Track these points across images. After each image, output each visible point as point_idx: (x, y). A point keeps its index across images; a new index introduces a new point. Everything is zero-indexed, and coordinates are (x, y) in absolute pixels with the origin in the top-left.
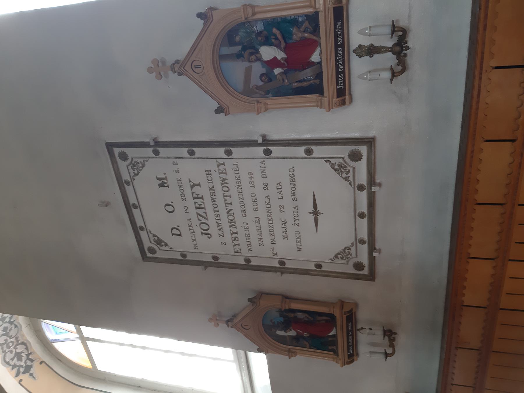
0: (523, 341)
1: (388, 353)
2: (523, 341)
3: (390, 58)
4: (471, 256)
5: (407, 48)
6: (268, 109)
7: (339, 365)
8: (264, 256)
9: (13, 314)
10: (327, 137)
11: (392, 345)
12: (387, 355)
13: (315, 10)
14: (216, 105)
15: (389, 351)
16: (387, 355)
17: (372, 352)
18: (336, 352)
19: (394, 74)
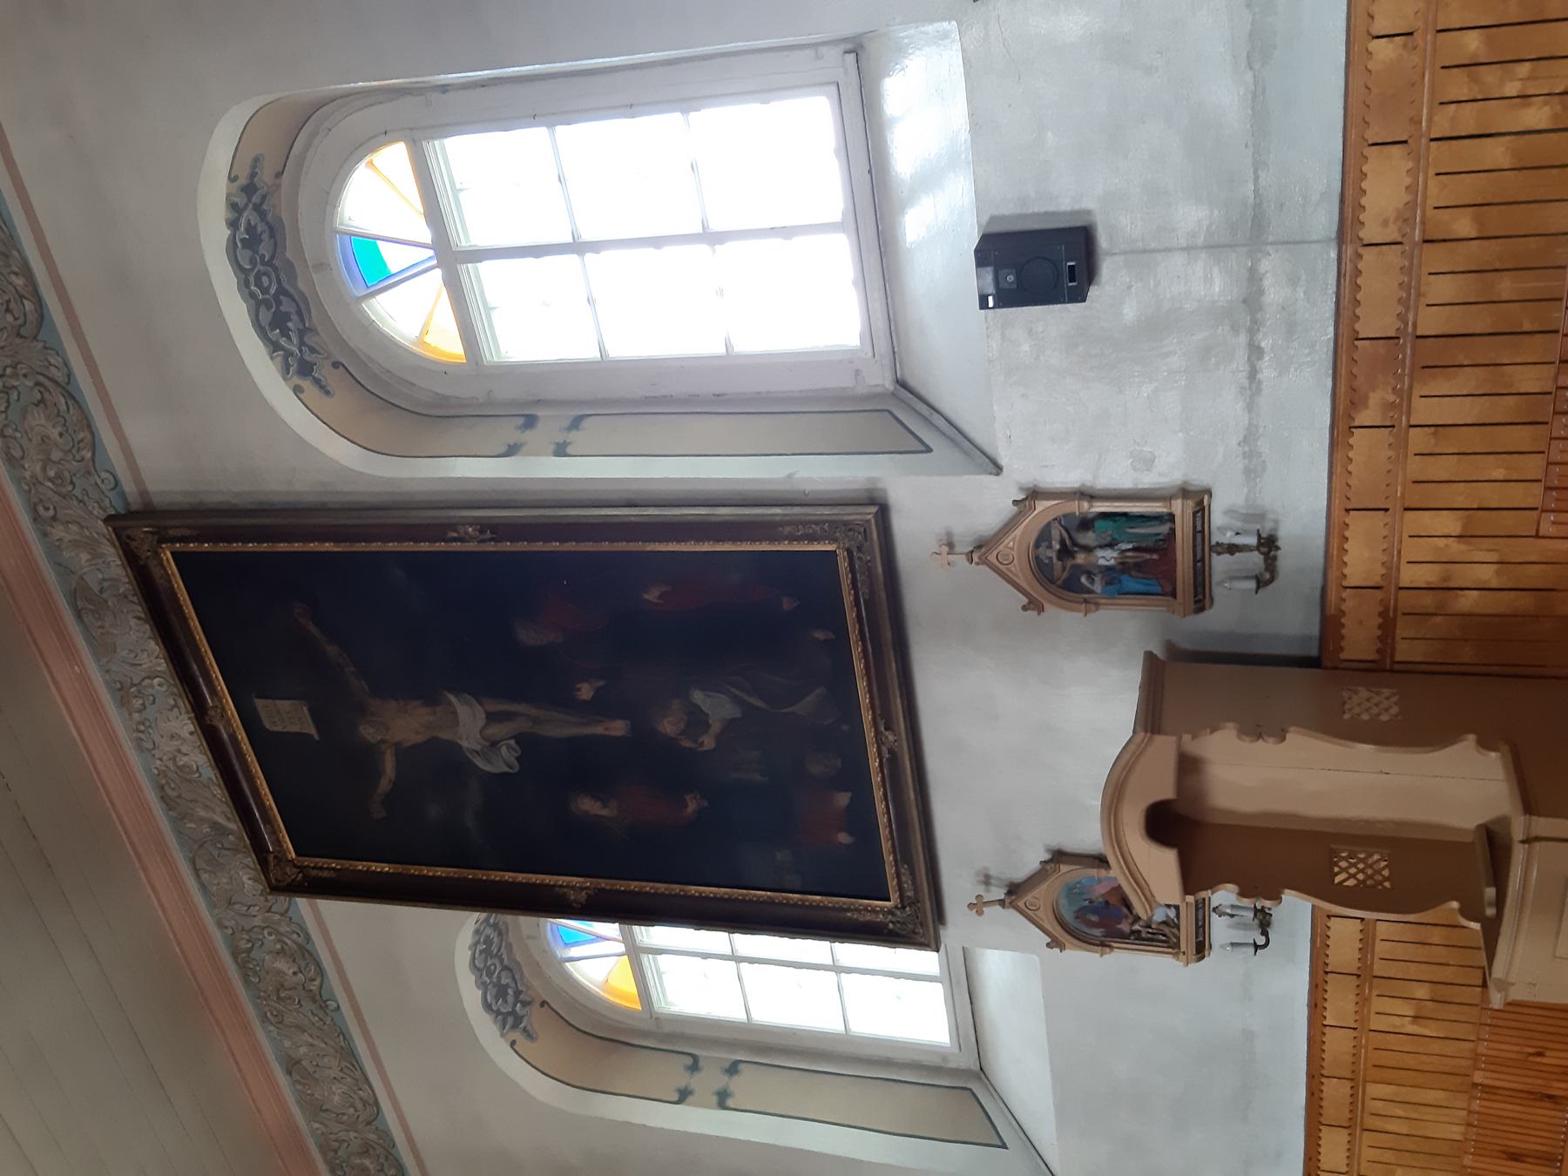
0: (1566, 959)
1: (1258, 943)
2: (1566, 959)
3: (1256, 559)
4: (1360, 337)
5: (1278, 548)
6: (902, 384)
7: (1182, 964)
8: (1470, 964)
9: (433, 877)
10: (1066, 488)
11: (1265, 933)
12: (1257, 947)
13: (1169, 511)
14: (1025, 600)
15: (1261, 940)
16: (1257, 947)
17: (1237, 944)
18: (1177, 946)
19: (1261, 583)
